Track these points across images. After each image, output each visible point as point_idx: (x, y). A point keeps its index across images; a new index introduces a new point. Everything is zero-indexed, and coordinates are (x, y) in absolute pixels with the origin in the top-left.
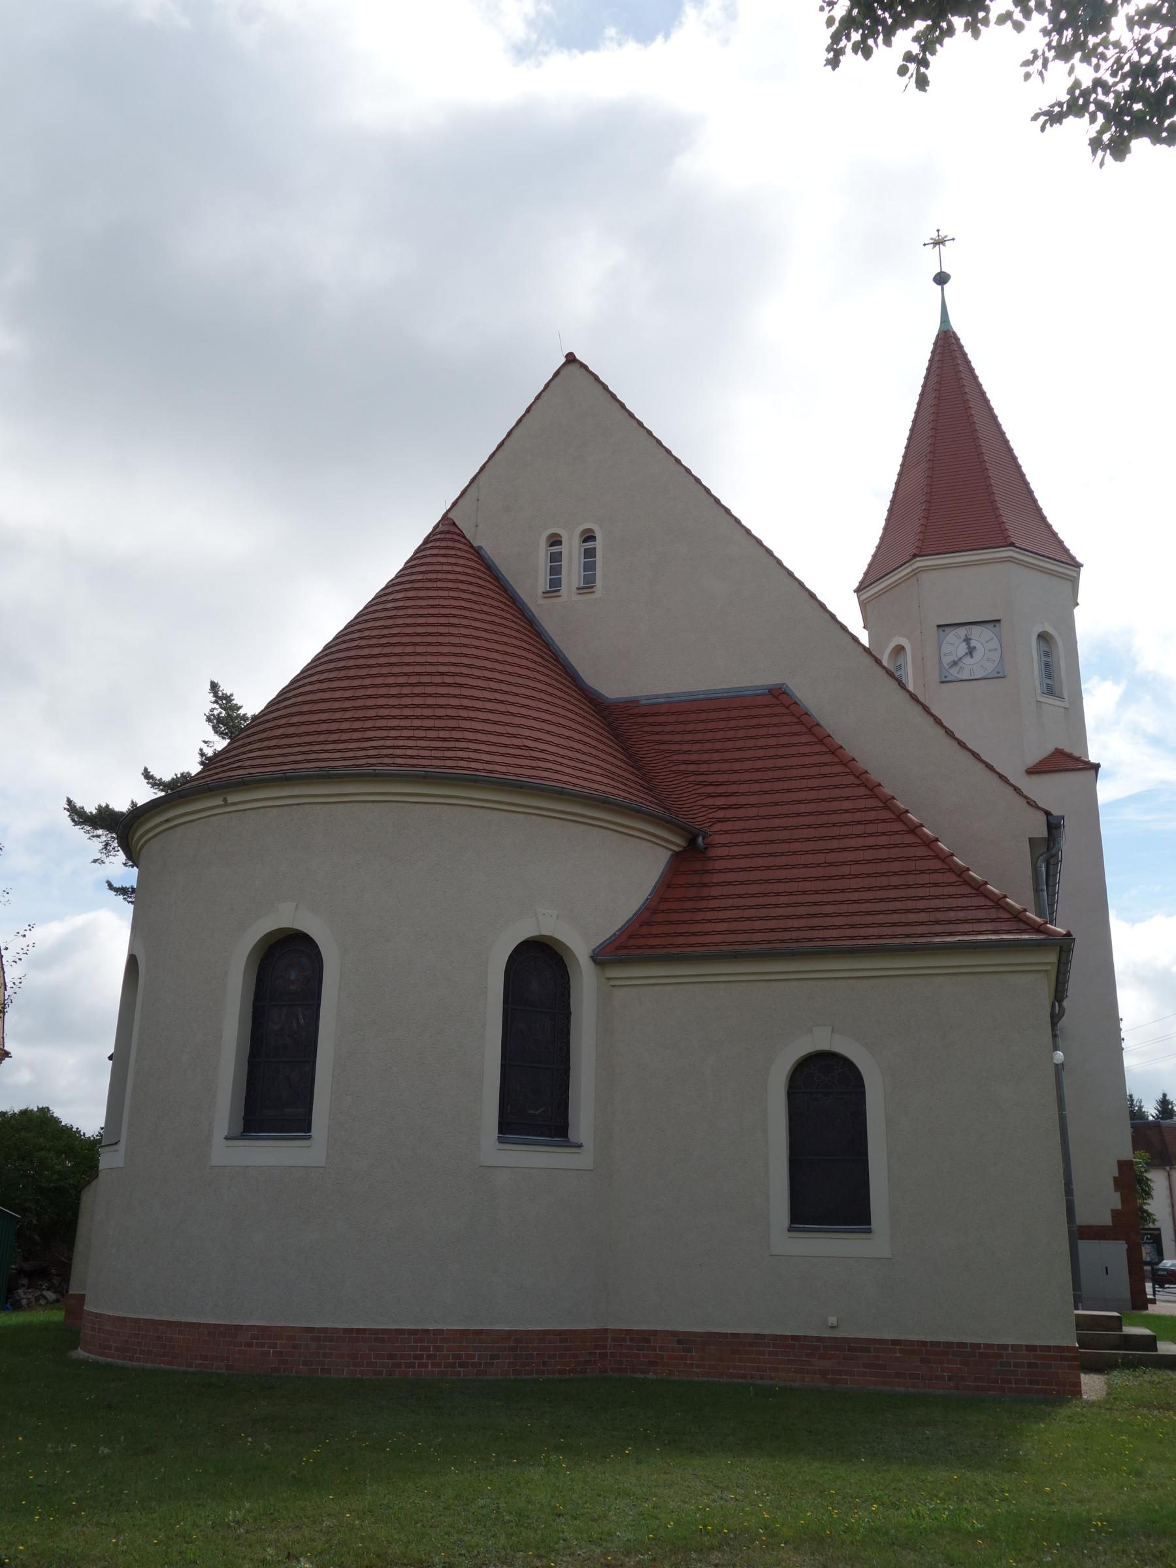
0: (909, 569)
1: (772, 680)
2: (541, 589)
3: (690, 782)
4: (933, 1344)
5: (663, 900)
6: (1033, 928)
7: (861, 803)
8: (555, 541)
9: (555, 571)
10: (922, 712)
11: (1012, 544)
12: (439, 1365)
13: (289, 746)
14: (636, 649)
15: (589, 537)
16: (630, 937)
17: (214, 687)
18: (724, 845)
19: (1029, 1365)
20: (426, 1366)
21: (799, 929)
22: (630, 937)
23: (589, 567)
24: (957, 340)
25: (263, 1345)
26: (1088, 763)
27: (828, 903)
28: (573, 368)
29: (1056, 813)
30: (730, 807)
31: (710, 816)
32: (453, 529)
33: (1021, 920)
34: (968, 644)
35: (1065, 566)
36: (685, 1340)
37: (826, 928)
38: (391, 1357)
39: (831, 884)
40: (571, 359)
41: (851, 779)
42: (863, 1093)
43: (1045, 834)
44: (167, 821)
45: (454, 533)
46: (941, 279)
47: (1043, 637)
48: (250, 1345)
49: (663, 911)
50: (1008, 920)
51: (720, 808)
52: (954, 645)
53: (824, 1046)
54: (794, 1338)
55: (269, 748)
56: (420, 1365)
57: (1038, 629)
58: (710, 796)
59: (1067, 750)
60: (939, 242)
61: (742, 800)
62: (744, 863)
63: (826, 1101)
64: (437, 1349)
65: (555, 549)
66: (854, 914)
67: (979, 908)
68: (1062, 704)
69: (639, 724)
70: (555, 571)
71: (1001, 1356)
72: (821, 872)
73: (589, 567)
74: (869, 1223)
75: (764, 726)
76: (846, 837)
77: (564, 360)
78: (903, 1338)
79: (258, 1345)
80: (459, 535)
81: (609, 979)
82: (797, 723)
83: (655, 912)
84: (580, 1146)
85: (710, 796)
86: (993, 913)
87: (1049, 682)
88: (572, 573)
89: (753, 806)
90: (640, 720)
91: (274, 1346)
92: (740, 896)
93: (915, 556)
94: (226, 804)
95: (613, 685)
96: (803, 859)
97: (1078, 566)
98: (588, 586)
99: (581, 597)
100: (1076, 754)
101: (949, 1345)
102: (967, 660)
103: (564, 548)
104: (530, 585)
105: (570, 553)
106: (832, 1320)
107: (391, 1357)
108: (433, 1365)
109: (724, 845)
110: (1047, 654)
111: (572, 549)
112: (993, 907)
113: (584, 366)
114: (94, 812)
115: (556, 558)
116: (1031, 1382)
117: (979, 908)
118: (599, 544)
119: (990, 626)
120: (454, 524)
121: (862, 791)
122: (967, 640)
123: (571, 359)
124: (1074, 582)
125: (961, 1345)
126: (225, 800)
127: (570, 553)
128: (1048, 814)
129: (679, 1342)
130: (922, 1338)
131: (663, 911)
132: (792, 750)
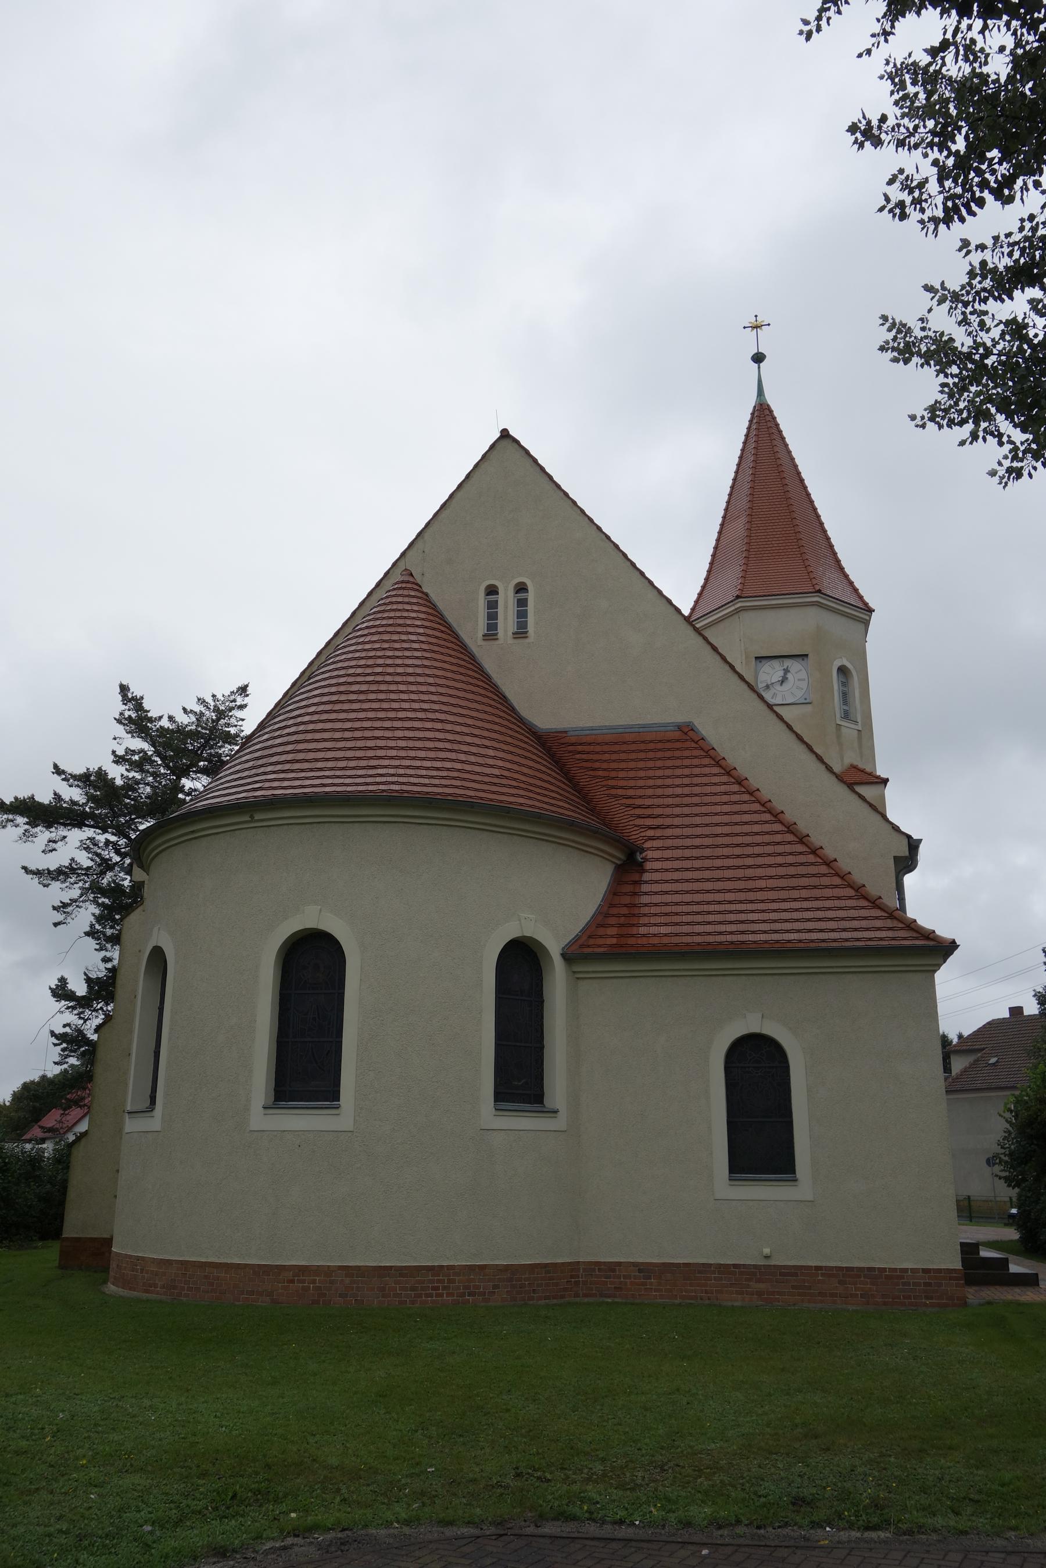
0: (733, 608)
1: (680, 719)
2: (480, 634)
3: (622, 805)
4: (848, 1269)
5: (612, 906)
6: (923, 936)
7: (767, 828)
8: (492, 591)
9: (492, 616)
10: (806, 750)
11: (819, 591)
12: (452, 1295)
13: (302, 771)
14: (563, 688)
15: (521, 588)
16: (590, 937)
17: (124, 689)
18: (657, 860)
19: (926, 1284)
20: (441, 1295)
21: (731, 933)
22: (590, 937)
23: (522, 615)
24: (771, 411)
25: (303, 1281)
26: (878, 777)
27: (752, 911)
28: (505, 442)
29: (915, 837)
30: (658, 827)
31: (642, 834)
32: (411, 579)
33: (912, 929)
34: (785, 674)
35: (861, 612)
36: (644, 1269)
37: (753, 932)
38: (413, 1289)
39: (751, 896)
40: (505, 434)
41: (757, 807)
42: (788, 1068)
43: (907, 854)
44: (193, 832)
45: (413, 583)
46: (758, 358)
47: (843, 670)
48: (292, 1281)
49: (613, 915)
50: (902, 929)
51: (650, 828)
52: (770, 673)
53: (755, 1029)
54: (735, 1266)
55: (283, 771)
56: (438, 1295)
57: (837, 663)
58: (639, 817)
59: (861, 766)
60: (756, 327)
61: (668, 821)
62: (676, 876)
63: (757, 1074)
64: (450, 1281)
65: (492, 598)
66: (775, 921)
67: (877, 918)
68: (856, 727)
69: (570, 752)
70: (492, 616)
71: (902, 1277)
72: (741, 885)
73: (522, 615)
74: (794, 1172)
75: (678, 758)
76: (759, 855)
77: (498, 435)
78: (824, 1264)
79: (299, 1281)
80: (413, 583)
81: (574, 972)
82: (705, 757)
83: (607, 915)
84: (556, 1112)
85: (639, 817)
86: (889, 923)
87: (845, 708)
88: (507, 622)
89: (677, 827)
90: (571, 748)
91: (314, 1282)
92: (677, 904)
93: (738, 597)
94: (252, 820)
95: (544, 720)
96: (761, 884)
97: (871, 611)
98: (521, 632)
99: (516, 641)
100: (868, 770)
101: (860, 1269)
102: (778, 687)
103: (501, 598)
104: (472, 630)
105: (506, 602)
106: (767, 1251)
107: (413, 1289)
108: (448, 1295)
109: (657, 860)
110: (844, 684)
111: (506, 599)
112: (888, 918)
113: (516, 442)
114: (1007, 1015)
115: (492, 605)
116: (927, 1298)
117: (877, 918)
118: (531, 597)
119: (800, 659)
120: (411, 575)
121: (767, 817)
122: (768, 687)
123: (505, 434)
124: (866, 623)
125: (870, 1269)
126: (252, 817)
127: (506, 602)
128: (909, 837)
129: (640, 1271)
130: (839, 1264)
131: (613, 915)
132: (705, 780)
